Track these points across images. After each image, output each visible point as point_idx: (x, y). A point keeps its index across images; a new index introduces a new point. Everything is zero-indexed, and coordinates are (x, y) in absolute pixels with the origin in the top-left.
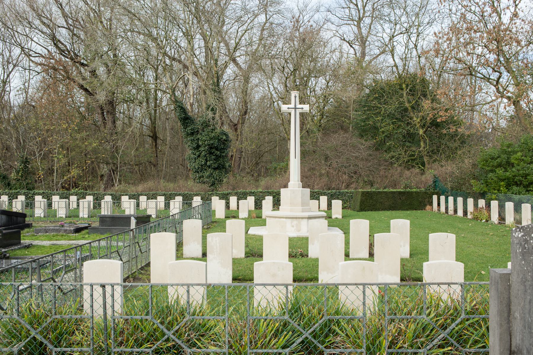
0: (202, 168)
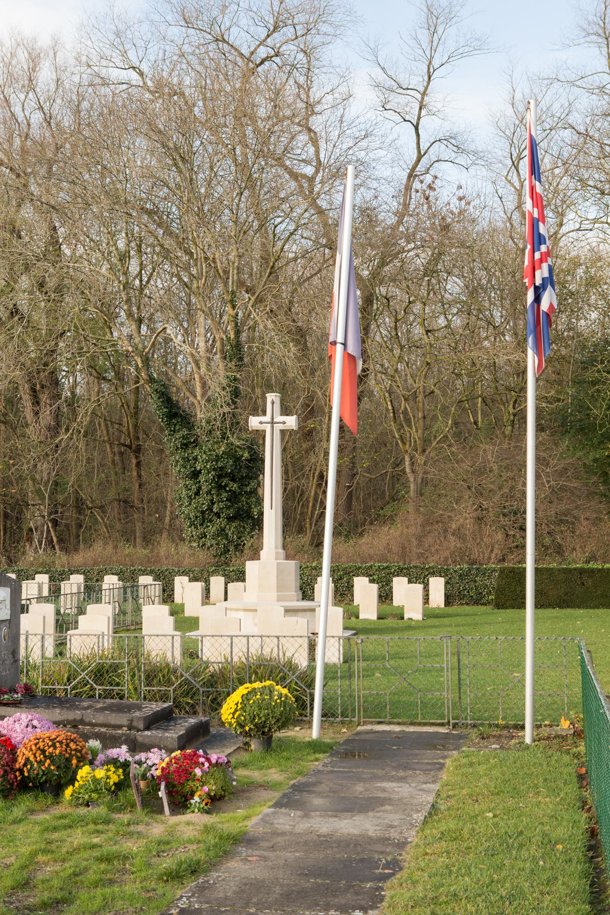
0: (204, 517)
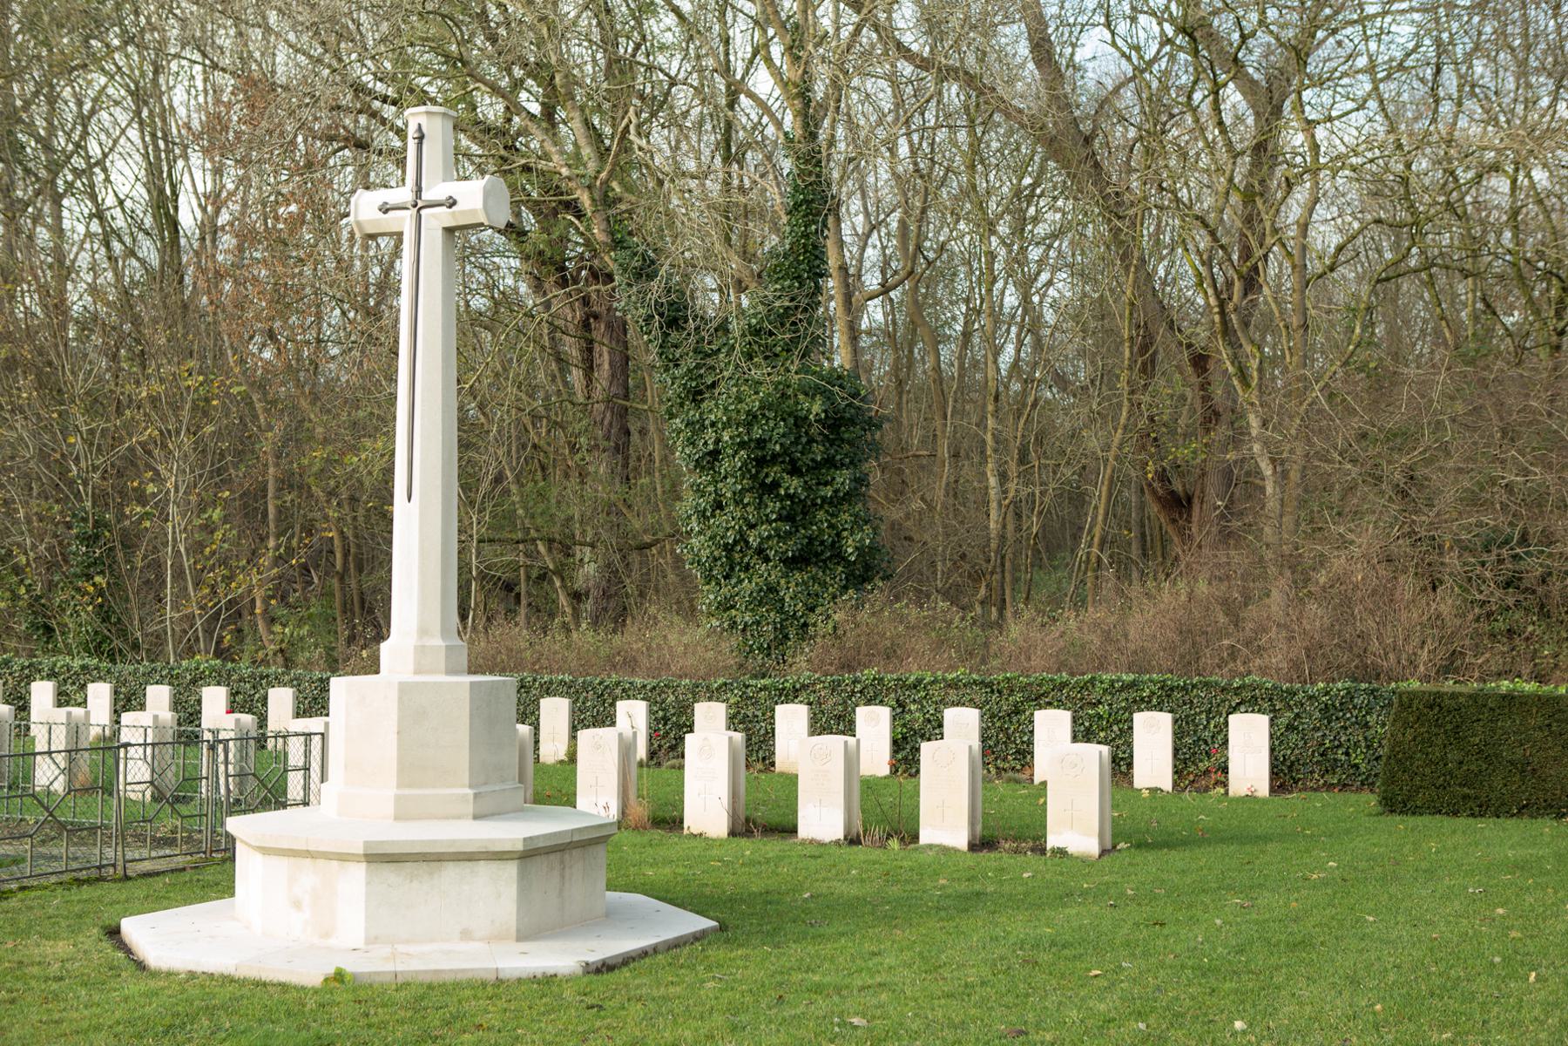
0: (732, 558)
